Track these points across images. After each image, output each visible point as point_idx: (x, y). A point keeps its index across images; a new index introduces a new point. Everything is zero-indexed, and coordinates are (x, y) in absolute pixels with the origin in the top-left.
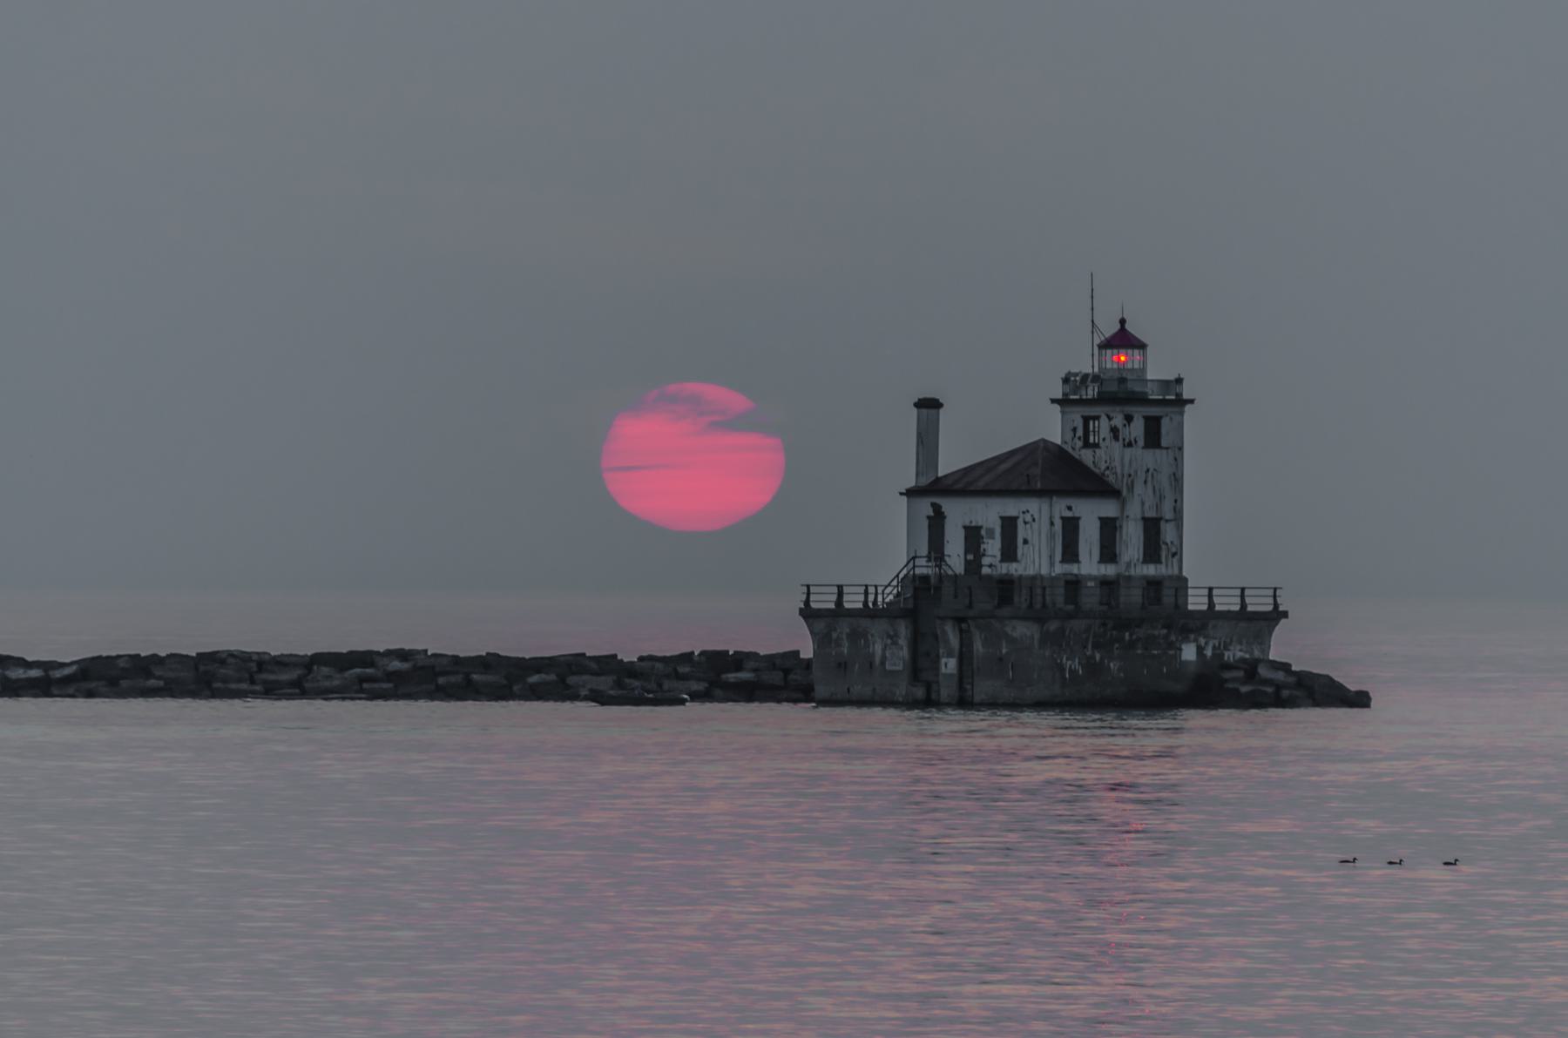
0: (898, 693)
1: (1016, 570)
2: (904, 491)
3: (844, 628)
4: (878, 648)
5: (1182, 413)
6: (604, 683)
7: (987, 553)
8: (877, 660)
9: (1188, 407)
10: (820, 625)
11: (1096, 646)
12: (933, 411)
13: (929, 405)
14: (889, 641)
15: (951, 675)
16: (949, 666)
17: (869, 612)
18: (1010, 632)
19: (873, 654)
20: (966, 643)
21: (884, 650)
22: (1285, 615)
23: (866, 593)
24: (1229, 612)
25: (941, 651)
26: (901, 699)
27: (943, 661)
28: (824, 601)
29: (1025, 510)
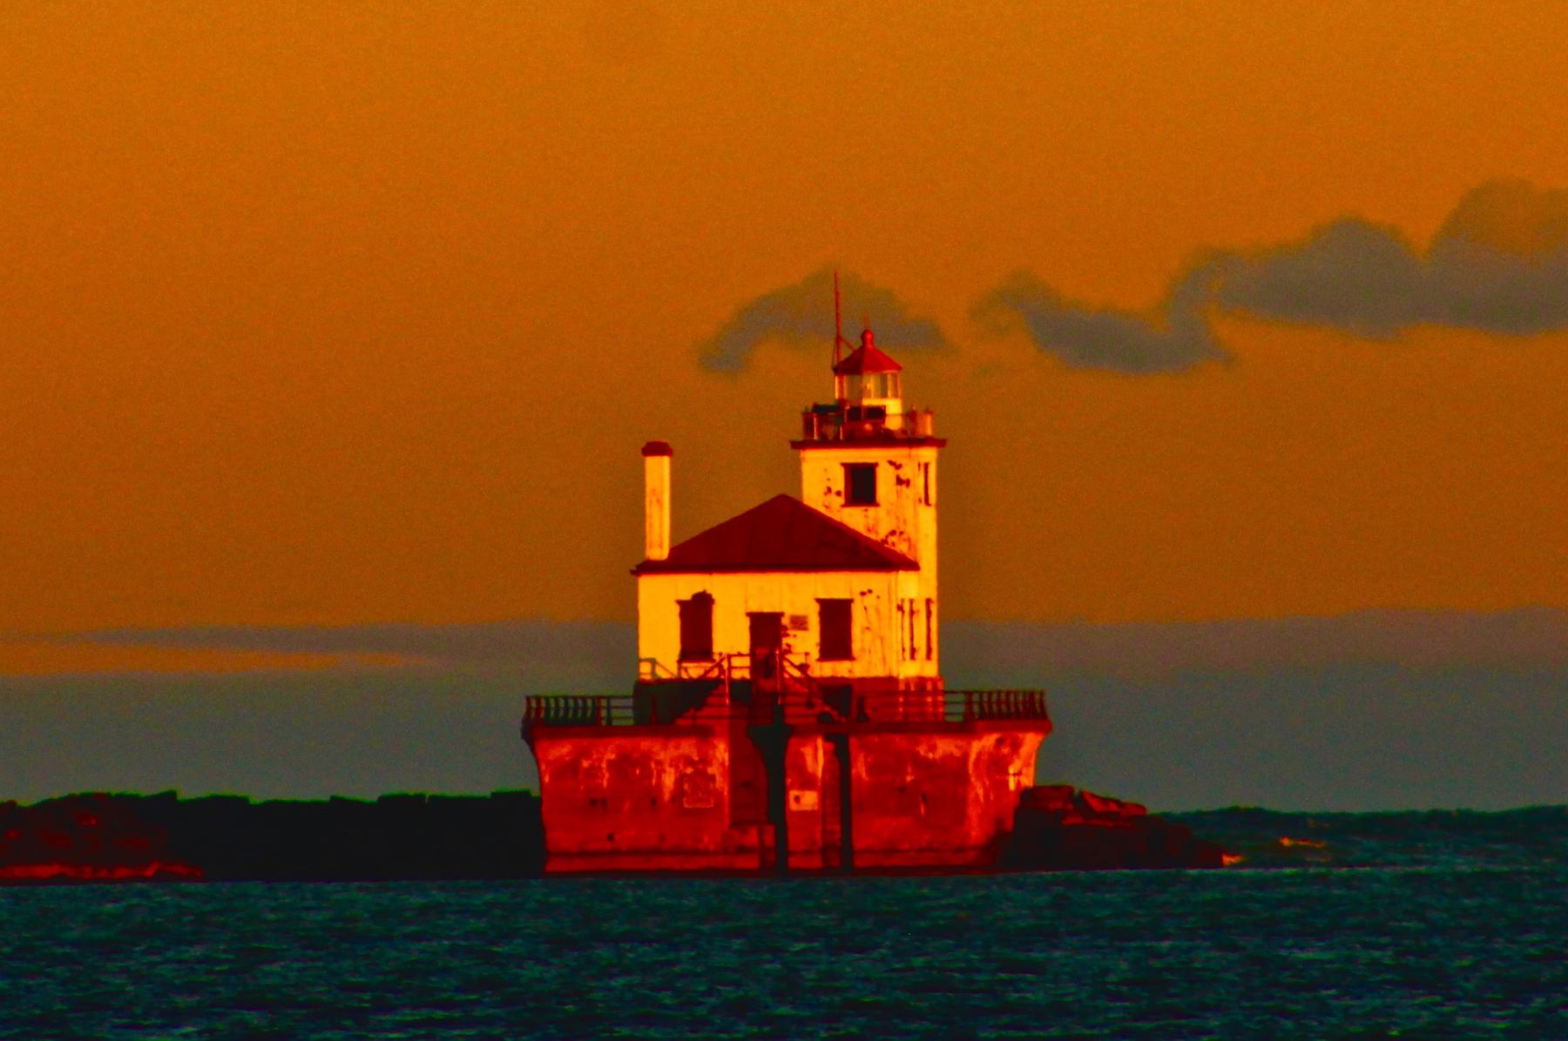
1: (850, 671)
2: (634, 568)
7: (793, 650)
18: (922, 753)
20: (840, 760)
23: (969, 704)
24: (461, 1028)
25: (789, 781)
26: (712, 847)
27: (793, 793)
29: (865, 590)
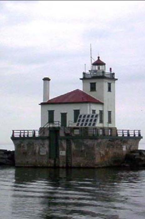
0: (44, 161)
3: (26, 142)
4: (37, 148)
5: (115, 83)
6: (79, 190)
8: (37, 152)
9: (116, 81)
10: (18, 142)
11: (107, 147)
12: (47, 81)
13: (46, 80)
14: (41, 146)
15: (63, 156)
16: (63, 153)
17: (128, 140)
19: (35, 150)
21: (39, 149)
22: (142, 138)
27: (61, 152)
28: (17, 135)
